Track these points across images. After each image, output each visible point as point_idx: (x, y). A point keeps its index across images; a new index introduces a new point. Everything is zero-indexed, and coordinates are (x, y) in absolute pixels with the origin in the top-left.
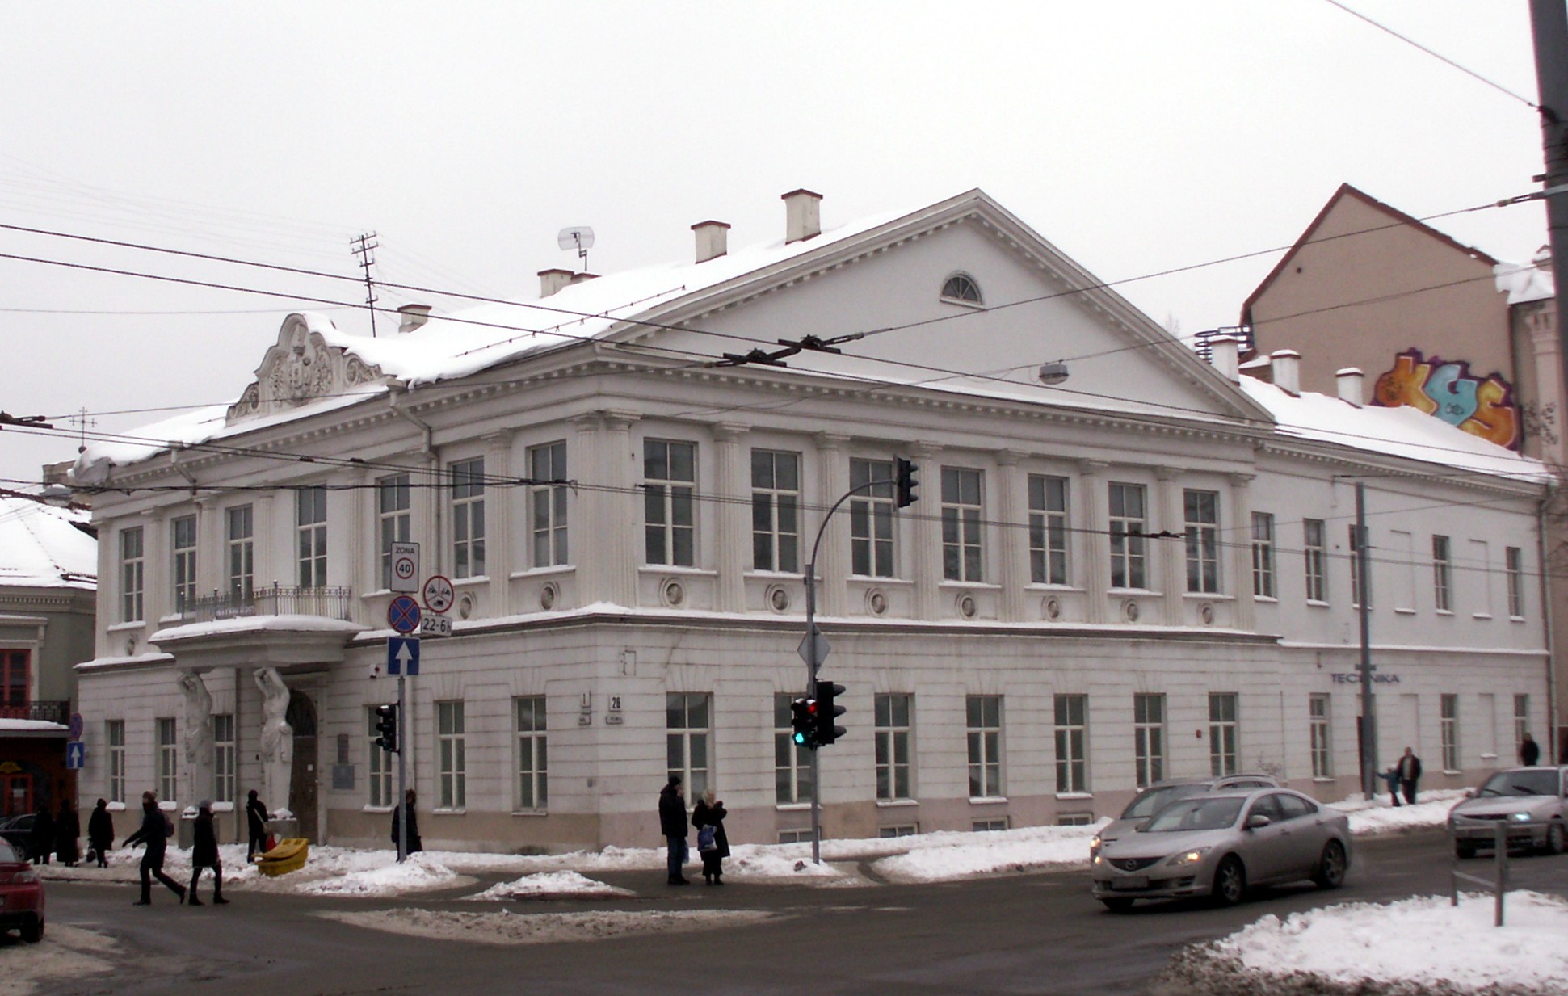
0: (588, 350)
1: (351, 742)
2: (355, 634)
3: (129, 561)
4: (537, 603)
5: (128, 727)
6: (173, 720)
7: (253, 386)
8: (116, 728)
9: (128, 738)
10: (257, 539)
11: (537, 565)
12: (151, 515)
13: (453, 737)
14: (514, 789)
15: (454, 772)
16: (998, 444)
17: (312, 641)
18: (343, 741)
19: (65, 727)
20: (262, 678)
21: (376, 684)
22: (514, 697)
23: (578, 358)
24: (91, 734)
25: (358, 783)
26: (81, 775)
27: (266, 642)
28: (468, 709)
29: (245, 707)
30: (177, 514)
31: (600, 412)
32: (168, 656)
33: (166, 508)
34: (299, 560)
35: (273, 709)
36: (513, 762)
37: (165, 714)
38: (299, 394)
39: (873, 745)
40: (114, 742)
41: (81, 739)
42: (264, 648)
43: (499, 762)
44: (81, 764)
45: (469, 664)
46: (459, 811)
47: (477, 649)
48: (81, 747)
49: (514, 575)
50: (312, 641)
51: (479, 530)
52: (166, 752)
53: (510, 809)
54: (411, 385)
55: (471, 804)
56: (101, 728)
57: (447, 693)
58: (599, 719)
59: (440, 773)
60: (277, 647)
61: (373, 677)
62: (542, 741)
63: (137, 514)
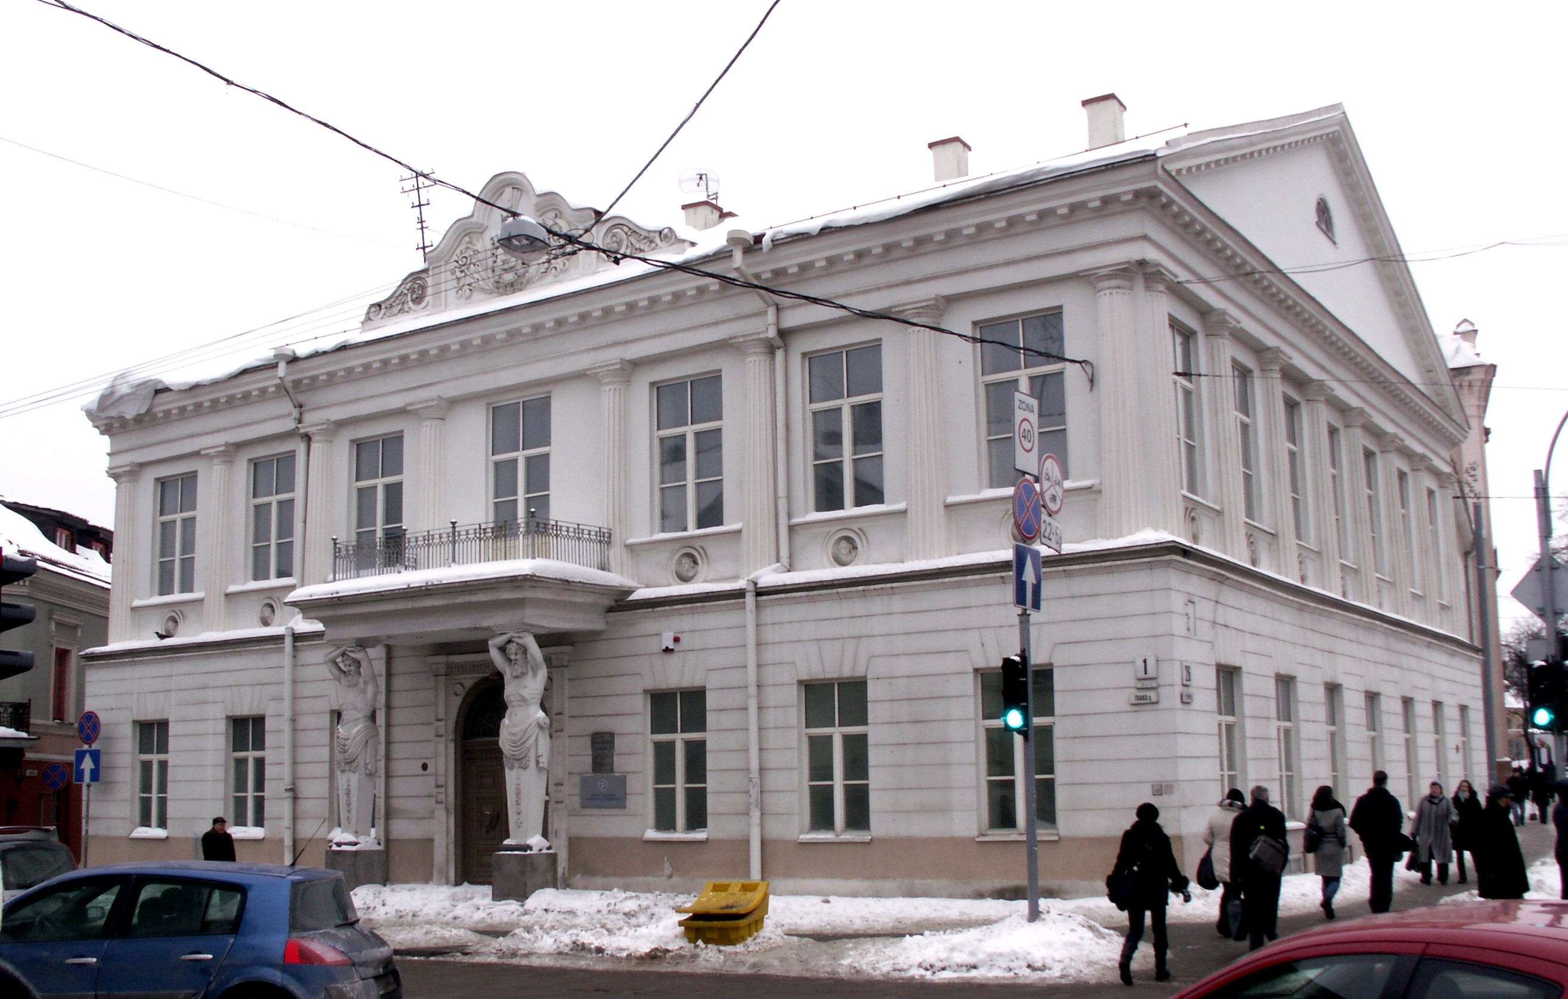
0: (1146, 168)
2: (630, 592)
3: (165, 518)
4: (257, 619)
5: (172, 729)
7: (416, 277)
8: (152, 733)
9: (172, 743)
10: (408, 478)
11: (256, 578)
12: (218, 455)
13: (155, 758)
15: (154, 795)
17: (580, 599)
19: (24, 735)
20: (502, 649)
21: (673, 660)
22: (135, 722)
25: (632, 802)
27: (528, 594)
28: (873, 691)
29: (397, 699)
30: (260, 452)
31: (1142, 263)
32: (319, 627)
33: (239, 446)
34: (492, 501)
35: (526, 693)
37: (244, 710)
38: (509, 277)
41: (95, 746)
42: (520, 603)
43: (947, 764)
44: (95, 775)
45: (878, 626)
46: (160, 833)
47: (897, 603)
48: (96, 756)
49: (951, 499)
50: (580, 599)
51: (188, 545)
53: (975, 833)
54: (766, 240)
55: (881, 824)
57: (676, 675)
58: (1170, 696)
60: (538, 602)
61: (667, 650)
62: (163, 765)
63: (196, 454)
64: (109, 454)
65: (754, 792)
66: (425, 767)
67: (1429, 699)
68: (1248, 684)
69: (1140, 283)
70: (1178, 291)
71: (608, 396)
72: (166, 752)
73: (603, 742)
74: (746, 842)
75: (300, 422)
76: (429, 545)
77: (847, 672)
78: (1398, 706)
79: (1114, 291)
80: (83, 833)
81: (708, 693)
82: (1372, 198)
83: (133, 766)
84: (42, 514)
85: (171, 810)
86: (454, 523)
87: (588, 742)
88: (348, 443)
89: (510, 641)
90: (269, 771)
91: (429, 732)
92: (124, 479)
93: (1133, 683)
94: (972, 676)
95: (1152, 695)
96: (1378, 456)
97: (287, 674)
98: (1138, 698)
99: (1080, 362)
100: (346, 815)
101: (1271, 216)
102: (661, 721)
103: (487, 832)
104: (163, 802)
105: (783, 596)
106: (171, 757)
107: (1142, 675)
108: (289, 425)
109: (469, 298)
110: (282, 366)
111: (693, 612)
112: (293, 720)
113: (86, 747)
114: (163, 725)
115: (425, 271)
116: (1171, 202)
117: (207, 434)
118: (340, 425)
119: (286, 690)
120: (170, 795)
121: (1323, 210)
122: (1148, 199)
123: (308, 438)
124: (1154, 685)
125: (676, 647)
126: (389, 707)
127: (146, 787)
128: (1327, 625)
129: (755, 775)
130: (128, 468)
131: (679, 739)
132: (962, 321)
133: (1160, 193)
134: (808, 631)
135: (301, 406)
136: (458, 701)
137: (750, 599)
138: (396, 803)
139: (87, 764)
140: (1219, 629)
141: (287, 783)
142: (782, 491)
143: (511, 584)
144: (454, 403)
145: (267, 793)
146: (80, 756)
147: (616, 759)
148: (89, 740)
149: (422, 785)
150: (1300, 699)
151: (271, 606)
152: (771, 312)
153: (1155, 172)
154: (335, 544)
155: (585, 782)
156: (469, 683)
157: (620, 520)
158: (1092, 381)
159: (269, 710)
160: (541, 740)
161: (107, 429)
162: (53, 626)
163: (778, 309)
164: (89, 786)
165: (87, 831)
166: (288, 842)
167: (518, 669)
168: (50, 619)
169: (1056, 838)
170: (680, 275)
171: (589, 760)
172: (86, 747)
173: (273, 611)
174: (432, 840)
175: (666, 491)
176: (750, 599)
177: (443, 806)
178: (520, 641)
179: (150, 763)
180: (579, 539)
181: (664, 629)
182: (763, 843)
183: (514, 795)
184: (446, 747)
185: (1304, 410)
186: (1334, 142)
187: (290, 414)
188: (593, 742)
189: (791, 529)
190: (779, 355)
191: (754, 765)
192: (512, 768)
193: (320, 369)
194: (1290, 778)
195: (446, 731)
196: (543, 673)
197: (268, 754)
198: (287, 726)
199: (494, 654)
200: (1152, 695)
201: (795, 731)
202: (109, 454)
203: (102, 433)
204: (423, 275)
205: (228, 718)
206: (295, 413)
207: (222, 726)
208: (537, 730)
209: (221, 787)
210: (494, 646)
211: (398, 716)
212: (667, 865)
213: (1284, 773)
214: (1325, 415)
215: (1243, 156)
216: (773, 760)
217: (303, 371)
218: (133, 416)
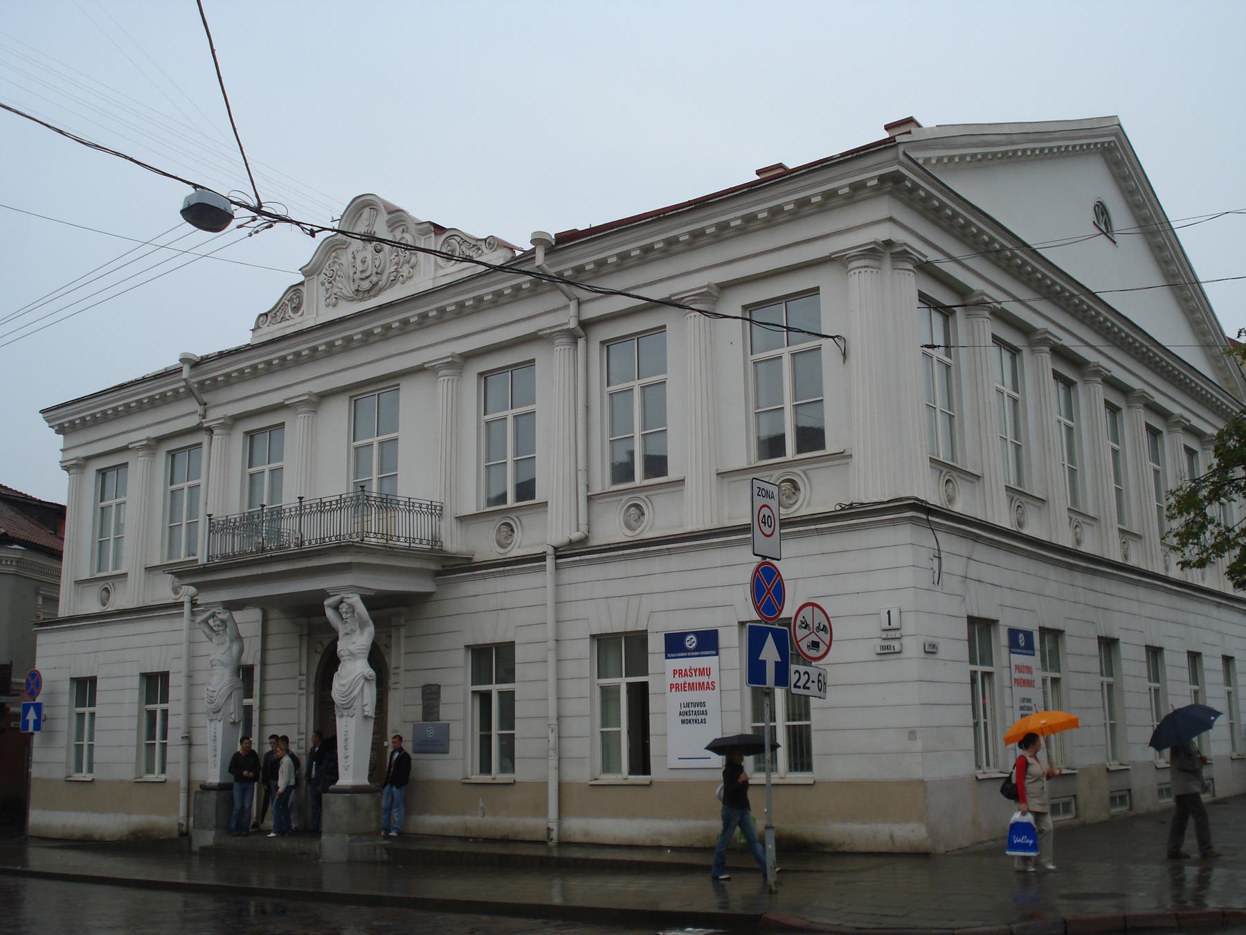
1: (445, 694)
5: (100, 685)
6: (165, 676)
7: (295, 289)
8: (85, 688)
14: (138, 758)
16: (1038, 323)
18: (431, 695)
20: (336, 608)
23: (582, 256)
24: (52, 694)
25: (455, 747)
26: (37, 738)
29: (272, 657)
31: (888, 243)
36: (742, 711)
38: (366, 285)
39: (518, 712)
40: (80, 702)
41: (38, 700)
44: (37, 726)
47: (675, 562)
48: (38, 708)
52: (152, 715)
56: (66, 686)
57: (489, 634)
59: (598, 729)
63: (124, 449)
65: (552, 737)
67: (1219, 653)
68: (1206, 662)
69: (887, 262)
70: (926, 269)
71: (443, 385)
74: (546, 784)
77: (631, 627)
78: (1219, 664)
79: (863, 270)
82: (1152, 204)
83: (70, 719)
84: (45, 508)
86: (301, 498)
87: (419, 692)
89: (341, 602)
93: (879, 634)
94: (736, 629)
95: (896, 644)
96: (1165, 434)
97: (184, 636)
98: (882, 647)
99: (833, 337)
101: (1046, 214)
102: (480, 675)
104: (91, 747)
106: (518, 687)
107: (886, 626)
108: (193, 421)
109: (334, 305)
110: (186, 368)
112: (189, 676)
115: (302, 283)
116: (916, 187)
120: (95, 743)
121: (1101, 211)
122: (893, 184)
124: (897, 634)
126: (263, 664)
127: (80, 735)
128: (1100, 583)
129: (553, 722)
131: (495, 688)
132: (733, 304)
133: (904, 177)
136: (318, 658)
137: (550, 562)
139: (32, 716)
140: (972, 584)
142: (581, 465)
144: (324, 396)
146: (26, 709)
150: (1068, 651)
152: (573, 304)
153: (897, 158)
155: (416, 728)
158: (844, 354)
160: (366, 690)
161: (61, 430)
162: (40, 600)
163: (579, 304)
166: (183, 784)
167: (349, 627)
168: (38, 594)
170: (501, 275)
175: (492, 469)
176: (550, 562)
178: (348, 601)
180: (409, 511)
182: (560, 785)
184: (308, 699)
185: (1080, 387)
186: (1107, 148)
188: (423, 694)
189: (590, 499)
190: (581, 342)
191: (552, 713)
192: (342, 716)
194: (1113, 726)
195: (308, 685)
196: (370, 630)
199: (330, 613)
200: (896, 644)
203: (58, 432)
204: (301, 287)
206: (200, 409)
207: (136, 682)
210: (329, 606)
211: (272, 672)
213: (1108, 722)
214: (1100, 393)
215: (1004, 154)
217: (206, 372)
218: (69, 418)
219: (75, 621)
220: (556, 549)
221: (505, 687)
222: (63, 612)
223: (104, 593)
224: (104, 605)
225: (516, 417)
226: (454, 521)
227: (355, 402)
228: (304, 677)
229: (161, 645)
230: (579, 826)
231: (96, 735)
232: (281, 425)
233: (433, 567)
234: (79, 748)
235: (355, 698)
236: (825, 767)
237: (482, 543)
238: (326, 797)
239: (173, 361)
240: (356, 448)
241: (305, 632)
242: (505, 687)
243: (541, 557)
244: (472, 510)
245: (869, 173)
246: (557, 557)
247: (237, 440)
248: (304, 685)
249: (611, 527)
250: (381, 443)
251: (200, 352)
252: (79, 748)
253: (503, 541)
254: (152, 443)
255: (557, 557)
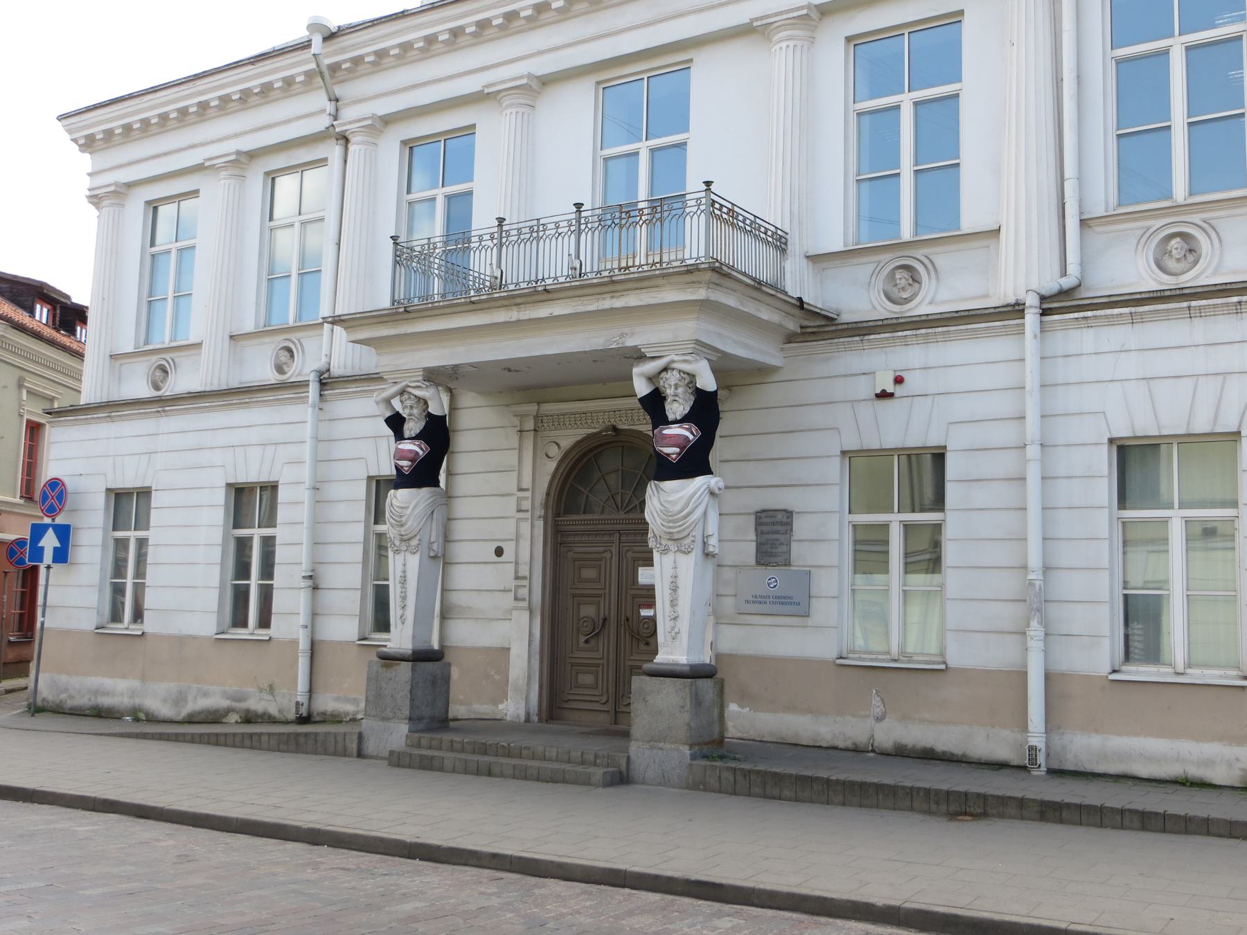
1: (801, 527)
8: (128, 504)
37: (250, 474)
41: (60, 520)
48: (64, 533)
56: (99, 500)
57: (900, 428)
61: (884, 395)
63: (198, 168)
64: (89, 174)
66: (499, 552)
71: (780, 57)
72: (147, 529)
73: (773, 524)
74: (1023, 676)
75: (336, 119)
76: (538, 239)
80: (38, 625)
81: (275, 592)
85: (149, 602)
88: (398, 144)
89: (665, 369)
90: (280, 554)
91: (512, 503)
92: (105, 203)
94: (1106, 447)
97: (307, 431)
100: (400, 612)
103: (587, 642)
104: (139, 590)
105: (1089, 314)
106: (152, 535)
108: (322, 123)
110: (317, 44)
111: (926, 340)
113: (47, 520)
114: (144, 494)
117: (212, 142)
118: (387, 121)
119: (306, 452)
120: (148, 581)
123: (345, 139)
125: (899, 390)
130: (112, 188)
134: (1130, 366)
135: (337, 100)
136: (552, 466)
137: (313, 389)
138: (457, 599)
139: (50, 542)
141: (304, 569)
143: (689, 278)
144: (547, 81)
145: (277, 582)
147: (794, 546)
148: (52, 511)
149: (501, 575)
151: (290, 351)
154: (396, 244)
156: (566, 443)
157: (800, 224)
159: (284, 476)
161: (88, 144)
164: (48, 567)
165: (43, 624)
166: (304, 645)
169: (943, 667)
171: (751, 548)
172: (47, 520)
173: (292, 356)
174: (509, 649)
176: (1031, 319)
177: (525, 604)
179: (127, 540)
181: (879, 362)
182: (1048, 677)
183: (667, 591)
184: (532, 526)
187: (324, 111)
188: (758, 524)
189: (1084, 223)
191: (1035, 561)
193: (364, 46)
197: (280, 533)
198: (305, 495)
201: (1106, 511)
202: (89, 174)
205: (229, 485)
206: (330, 107)
207: (220, 497)
208: (707, 498)
209: (216, 570)
210: (642, 375)
212: (876, 701)
216: (1066, 555)
217: (343, 50)
218: (102, 128)
219: (111, 408)
220: (1043, 299)
221: (267, 532)
222: (87, 396)
223: (159, 373)
224: (157, 388)
225: (653, 151)
226: (805, 260)
227: (604, 87)
228: (528, 494)
229: (265, 442)
230: (1084, 747)
231: (150, 570)
232: (470, 130)
233: (792, 326)
234: (118, 590)
235: (695, 523)
236: (150, 624)
237: (855, 296)
238: (638, 682)
239: (299, 33)
240: (606, 160)
241: (530, 425)
242: (267, 532)
243: (1016, 310)
244: (836, 243)
245: (299, 66)
246: (1045, 312)
247: (390, 153)
248: (527, 505)
249: (1128, 267)
250: (653, 151)
251: (334, 23)
252: (118, 590)
253: (895, 293)
254: (535, 85)
255: (1045, 312)
